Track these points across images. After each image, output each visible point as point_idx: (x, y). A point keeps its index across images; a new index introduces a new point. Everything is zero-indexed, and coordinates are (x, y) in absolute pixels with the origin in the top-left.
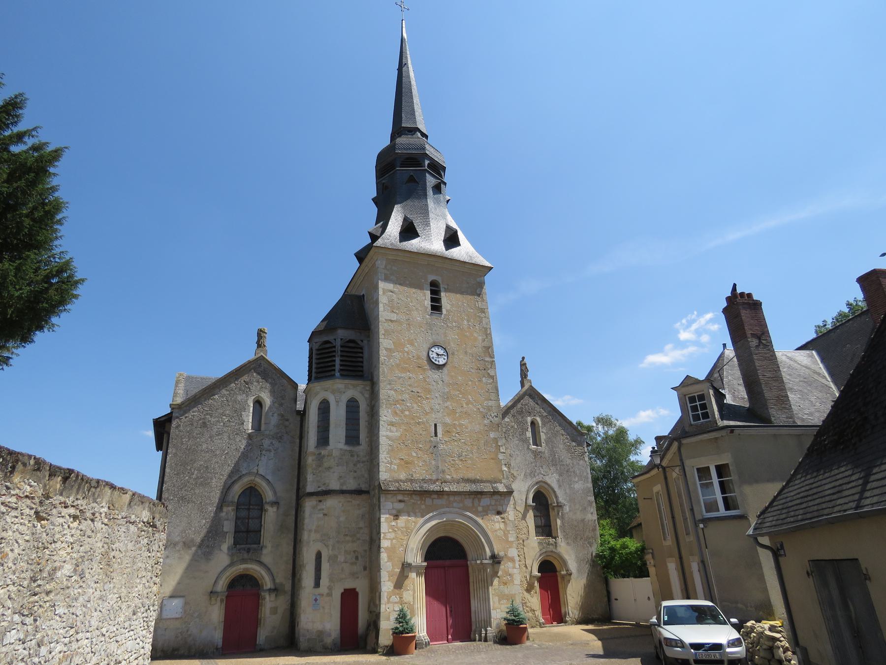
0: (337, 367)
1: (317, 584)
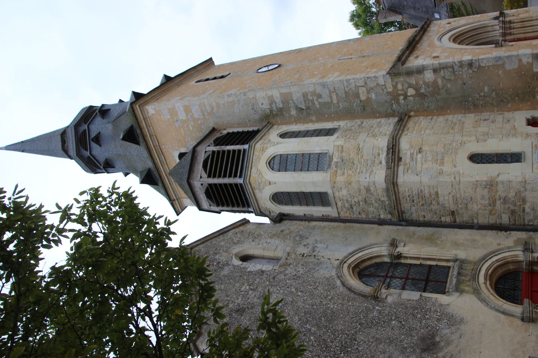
1: (516, 158)
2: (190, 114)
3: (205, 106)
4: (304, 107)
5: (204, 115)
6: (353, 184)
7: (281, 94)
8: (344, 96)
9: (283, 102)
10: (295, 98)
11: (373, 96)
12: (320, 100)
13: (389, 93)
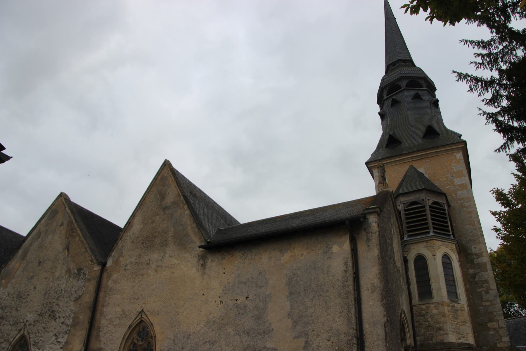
2: (460, 189)
3: (468, 201)
4: (476, 280)
5: (461, 199)
6: (443, 319)
7: (485, 263)
8: (489, 311)
9: (478, 264)
10: (483, 273)
11: (492, 332)
12: (483, 292)
13: (495, 344)
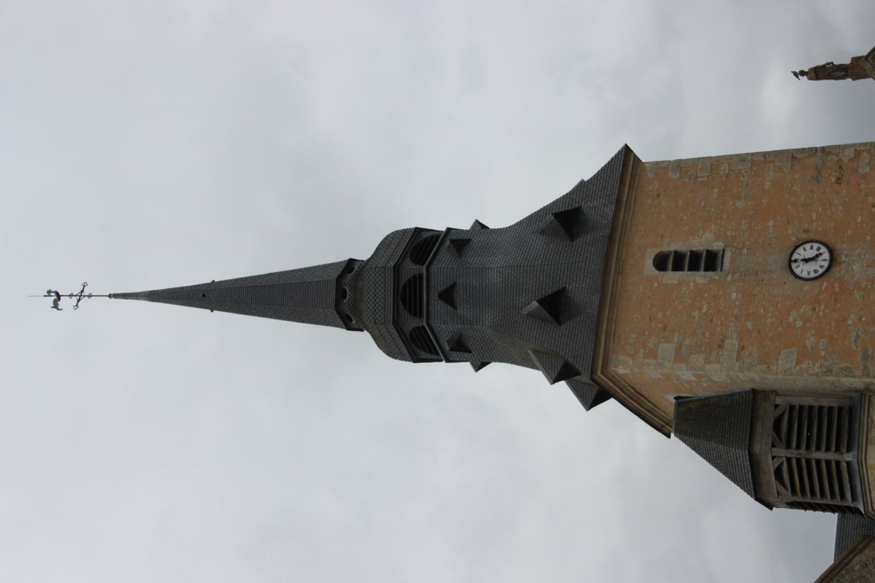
0: (832, 456)
